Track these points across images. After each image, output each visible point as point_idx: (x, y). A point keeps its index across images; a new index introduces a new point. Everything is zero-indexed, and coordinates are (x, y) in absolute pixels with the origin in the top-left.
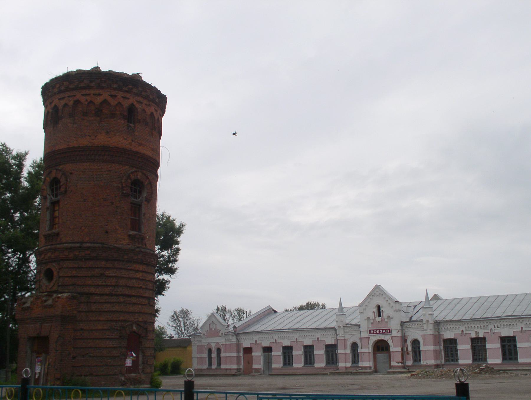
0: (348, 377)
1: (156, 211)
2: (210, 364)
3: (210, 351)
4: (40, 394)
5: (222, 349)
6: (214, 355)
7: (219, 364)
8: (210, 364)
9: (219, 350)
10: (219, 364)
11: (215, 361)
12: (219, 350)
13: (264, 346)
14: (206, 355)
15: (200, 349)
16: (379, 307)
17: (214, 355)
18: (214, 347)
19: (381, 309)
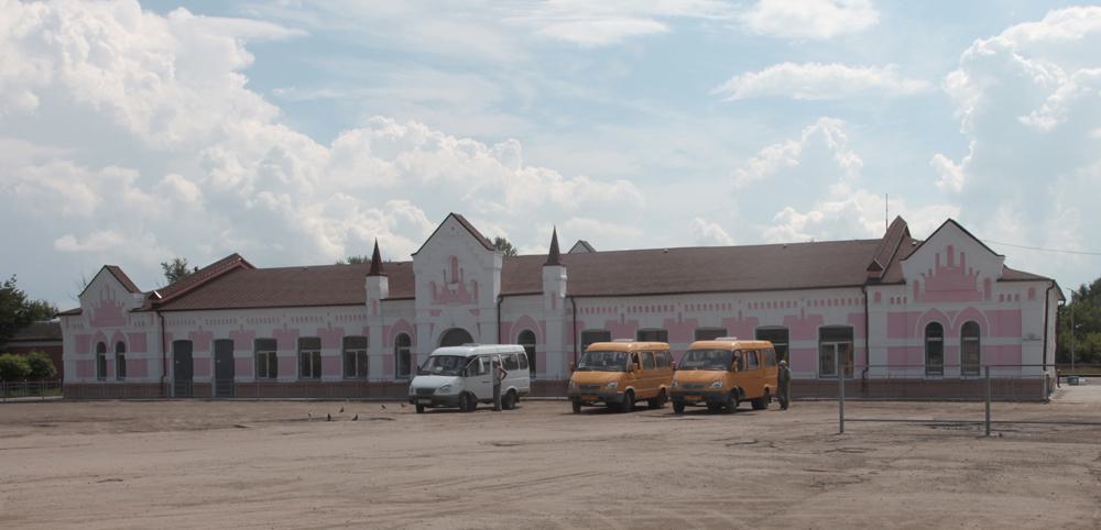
0: (182, 433)
1: (339, 266)
2: (103, 372)
3: (102, 347)
4: (46, 366)
5: (128, 345)
6: (110, 356)
7: (122, 372)
8: (103, 372)
9: (121, 347)
10: (122, 372)
11: (112, 367)
12: (121, 347)
13: (258, 336)
14: (92, 355)
15: (82, 342)
16: (454, 260)
17: (110, 356)
18: (895, 304)
19: (460, 266)
